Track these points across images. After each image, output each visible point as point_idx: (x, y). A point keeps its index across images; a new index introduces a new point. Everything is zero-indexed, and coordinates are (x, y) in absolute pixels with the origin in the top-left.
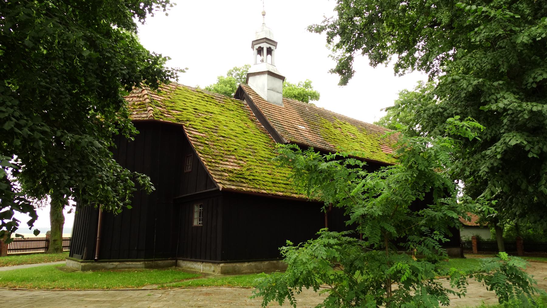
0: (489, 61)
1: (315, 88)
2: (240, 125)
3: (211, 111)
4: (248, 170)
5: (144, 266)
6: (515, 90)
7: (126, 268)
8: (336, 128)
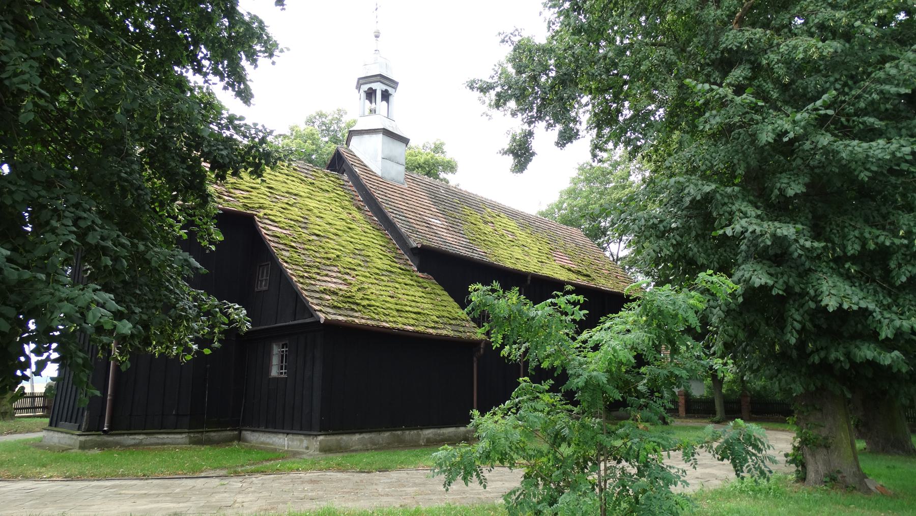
1: (449, 154)
2: (341, 216)
3: (296, 192)
4: (359, 290)
5: (187, 440)
6: (751, 198)
8: (486, 223)
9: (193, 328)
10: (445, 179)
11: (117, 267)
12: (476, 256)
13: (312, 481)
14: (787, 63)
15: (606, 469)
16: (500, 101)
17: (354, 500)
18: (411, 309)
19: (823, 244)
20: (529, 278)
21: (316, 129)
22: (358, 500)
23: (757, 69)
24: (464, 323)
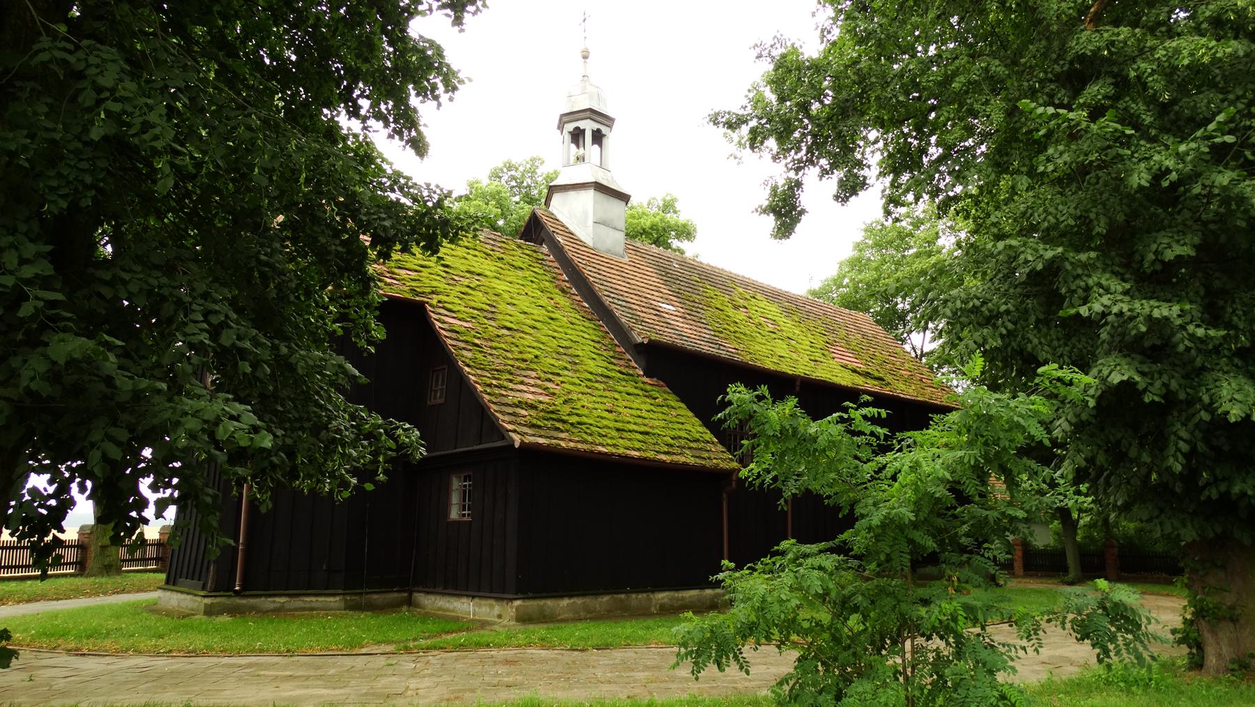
0: (1072, 211)
1: (684, 215)
3: (479, 271)
4: (565, 402)
5: (343, 605)
7: (304, 609)
8: (736, 307)
9: (350, 455)
10: (679, 250)
11: (257, 374)
12: (723, 354)
13: (507, 662)
14: (1166, 75)
15: (914, 652)
16: (756, 139)
17: (564, 689)
18: (635, 428)
19: (1223, 333)
20: (798, 383)
21: (503, 184)
22: (570, 688)
23: (1123, 86)
24: (708, 447)
